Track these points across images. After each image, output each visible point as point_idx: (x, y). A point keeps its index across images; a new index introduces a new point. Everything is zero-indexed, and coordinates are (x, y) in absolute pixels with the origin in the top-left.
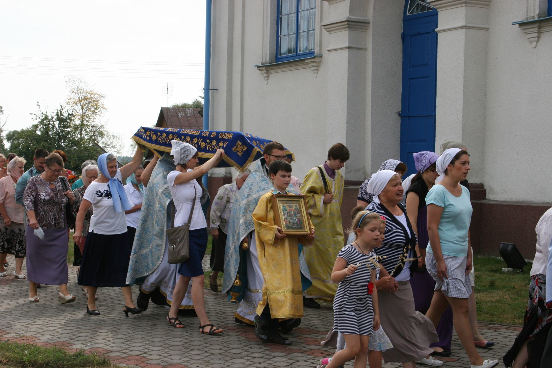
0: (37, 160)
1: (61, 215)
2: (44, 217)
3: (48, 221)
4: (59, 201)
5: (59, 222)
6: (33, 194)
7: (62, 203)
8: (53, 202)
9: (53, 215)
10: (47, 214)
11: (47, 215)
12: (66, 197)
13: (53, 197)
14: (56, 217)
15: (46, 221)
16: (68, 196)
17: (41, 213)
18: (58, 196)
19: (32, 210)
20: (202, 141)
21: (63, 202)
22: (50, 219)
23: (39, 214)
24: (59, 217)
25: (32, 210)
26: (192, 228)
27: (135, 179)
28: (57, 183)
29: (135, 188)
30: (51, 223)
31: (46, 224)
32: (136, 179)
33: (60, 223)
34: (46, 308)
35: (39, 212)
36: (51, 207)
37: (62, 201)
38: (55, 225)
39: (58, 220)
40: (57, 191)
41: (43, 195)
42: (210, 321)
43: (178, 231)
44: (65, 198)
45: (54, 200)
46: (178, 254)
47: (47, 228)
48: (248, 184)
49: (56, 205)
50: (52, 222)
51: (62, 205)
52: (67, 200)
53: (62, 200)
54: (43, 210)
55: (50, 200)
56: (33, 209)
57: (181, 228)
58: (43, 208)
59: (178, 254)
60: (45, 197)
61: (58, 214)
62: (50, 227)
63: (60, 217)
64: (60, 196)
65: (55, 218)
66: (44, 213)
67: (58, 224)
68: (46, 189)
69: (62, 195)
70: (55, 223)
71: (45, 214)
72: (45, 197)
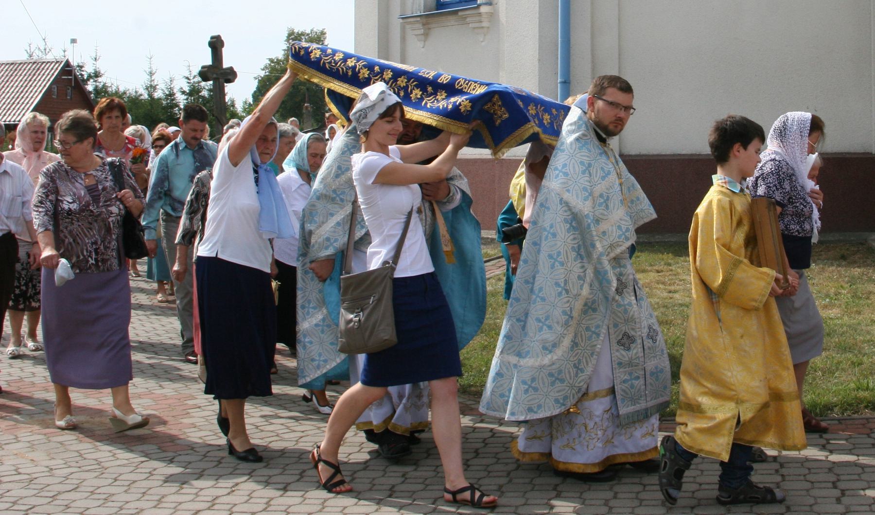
0: (186, 124)
1: (109, 243)
2: (72, 247)
3: (82, 257)
4: (102, 212)
5: (105, 257)
6: (50, 198)
7: (110, 217)
8: (90, 216)
9: (93, 243)
10: (79, 241)
11: (78, 243)
12: (118, 203)
13: (88, 205)
14: (99, 248)
15: (78, 257)
16: (125, 202)
17: (67, 240)
18: (100, 202)
19: (49, 230)
20: (415, 86)
21: (112, 213)
22: (85, 253)
23: (63, 241)
24: (106, 248)
25: (49, 230)
26: (398, 274)
27: (306, 162)
28: (101, 173)
29: (303, 180)
30: (88, 261)
31: (78, 262)
32: (309, 161)
33: (107, 260)
34: (48, 474)
35: (63, 238)
36: (88, 225)
37: (108, 211)
38: (97, 265)
39: (103, 254)
40: (98, 190)
41: (68, 202)
42: (671, 270)
43: (368, 282)
44: (115, 205)
45: (92, 211)
46: (371, 333)
47: (81, 270)
48: (556, 169)
49: (96, 221)
50: (90, 259)
51: (110, 219)
52: (120, 209)
53: (110, 209)
54: (70, 232)
55: (82, 210)
56: (51, 227)
57: (372, 277)
58: (68, 228)
59: (371, 333)
60: (71, 206)
61: (102, 242)
62: (87, 269)
63: (109, 248)
64: (106, 202)
65: (96, 250)
66: (71, 240)
67: (104, 261)
68: (76, 188)
69: (110, 200)
70: (96, 260)
71: (74, 241)
72: (71, 206)
